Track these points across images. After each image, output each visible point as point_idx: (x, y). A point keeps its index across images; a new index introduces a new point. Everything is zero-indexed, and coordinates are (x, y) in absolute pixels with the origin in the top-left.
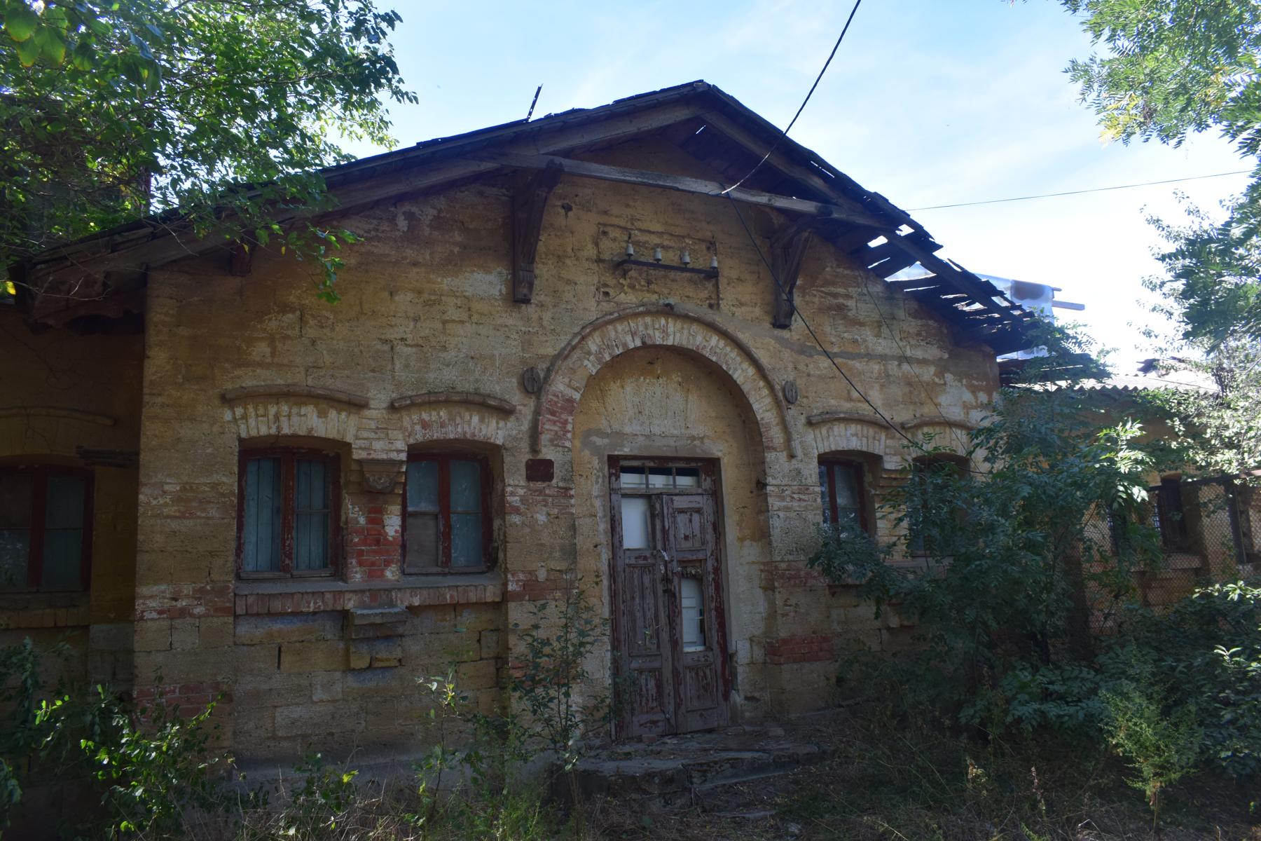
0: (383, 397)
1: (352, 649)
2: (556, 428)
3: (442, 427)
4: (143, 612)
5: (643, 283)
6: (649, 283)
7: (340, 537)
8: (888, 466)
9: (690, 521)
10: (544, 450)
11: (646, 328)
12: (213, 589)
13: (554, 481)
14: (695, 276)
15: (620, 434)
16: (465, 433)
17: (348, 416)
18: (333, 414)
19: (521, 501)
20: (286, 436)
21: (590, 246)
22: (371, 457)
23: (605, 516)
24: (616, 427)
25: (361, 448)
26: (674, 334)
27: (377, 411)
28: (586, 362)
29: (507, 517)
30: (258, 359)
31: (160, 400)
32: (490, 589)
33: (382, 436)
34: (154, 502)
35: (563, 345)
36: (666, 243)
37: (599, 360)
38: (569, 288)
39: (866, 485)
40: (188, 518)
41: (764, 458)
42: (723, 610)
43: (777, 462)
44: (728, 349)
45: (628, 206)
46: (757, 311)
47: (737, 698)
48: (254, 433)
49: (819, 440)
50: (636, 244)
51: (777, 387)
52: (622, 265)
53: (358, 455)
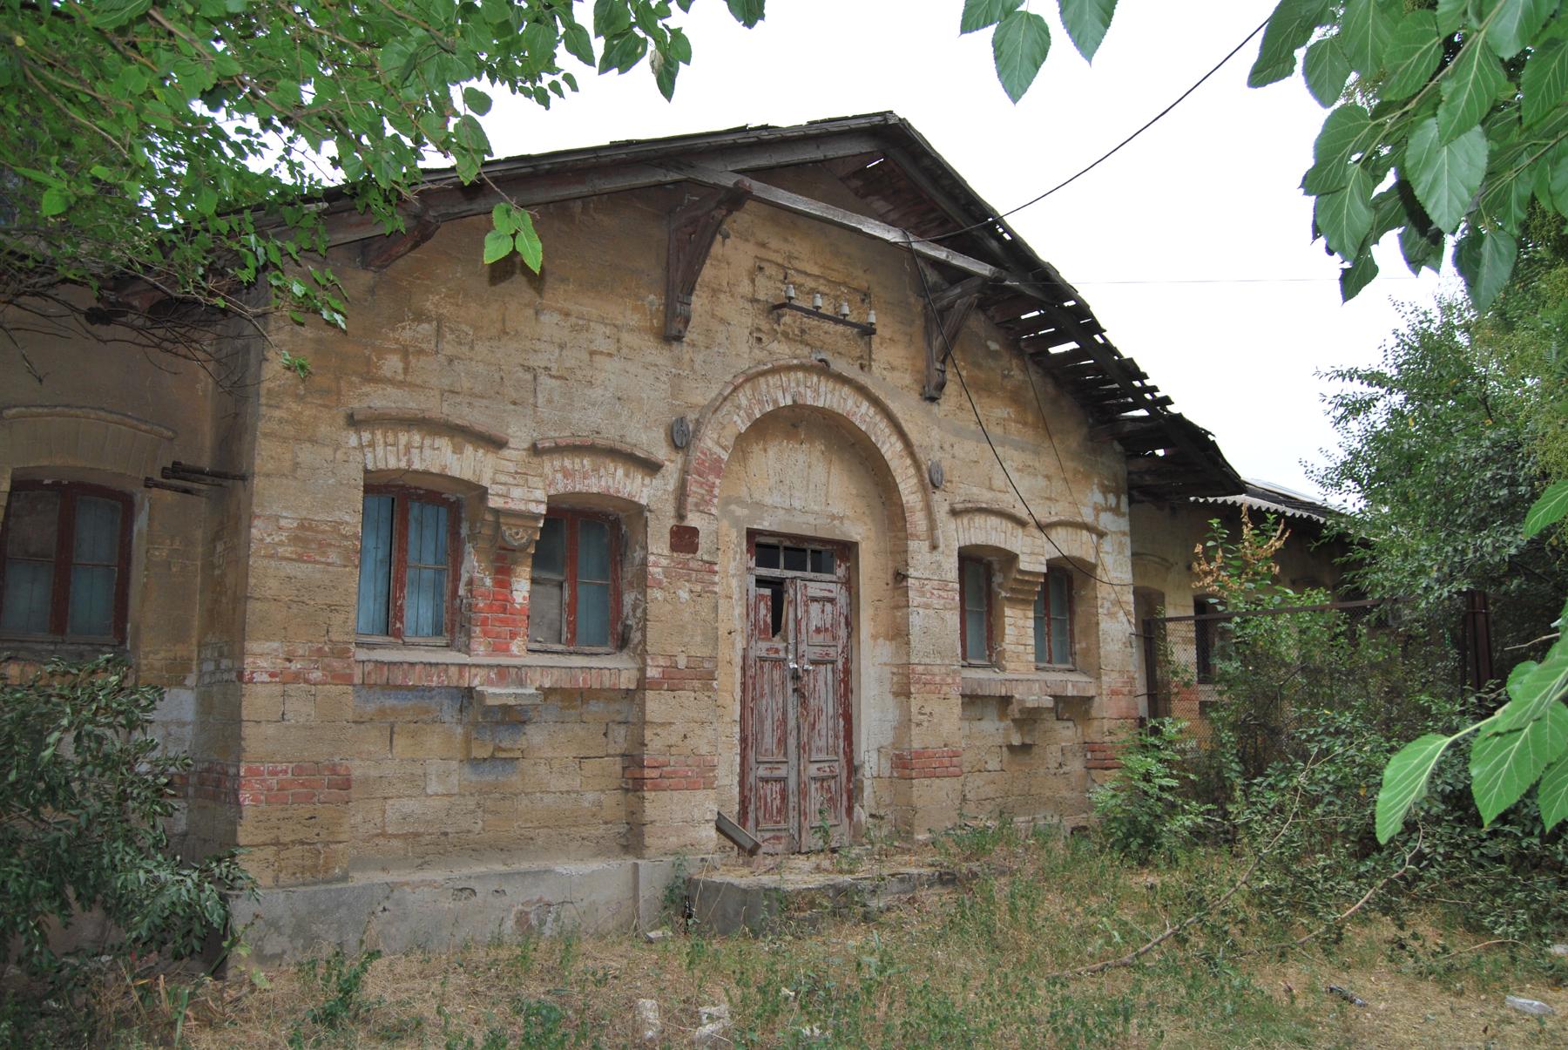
3: (585, 478)
4: (252, 673)
7: (458, 601)
8: (1023, 566)
9: (823, 611)
10: (690, 516)
11: (798, 385)
12: (332, 650)
14: (849, 331)
17: (485, 455)
18: (469, 449)
19: (664, 573)
20: (416, 472)
21: (746, 282)
22: (507, 506)
23: (740, 599)
24: (757, 496)
26: (825, 396)
27: (515, 453)
28: (736, 418)
29: (649, 591)
30: (389, 375)
31: (277, 413)
33: (522, 482)
34: (268, 540)
36: (822, 288)
38: (722, 328)
39: (995, 586)
40: (305, 562)
42: (851, 716)
43: (918, 548)
44: (878, 418)
45: (786, 240)
46: (907, 379)
47: (861, 814)
48: (382, 465)
49: (960, 530)
50: (798, 287)
53: (494, 502)
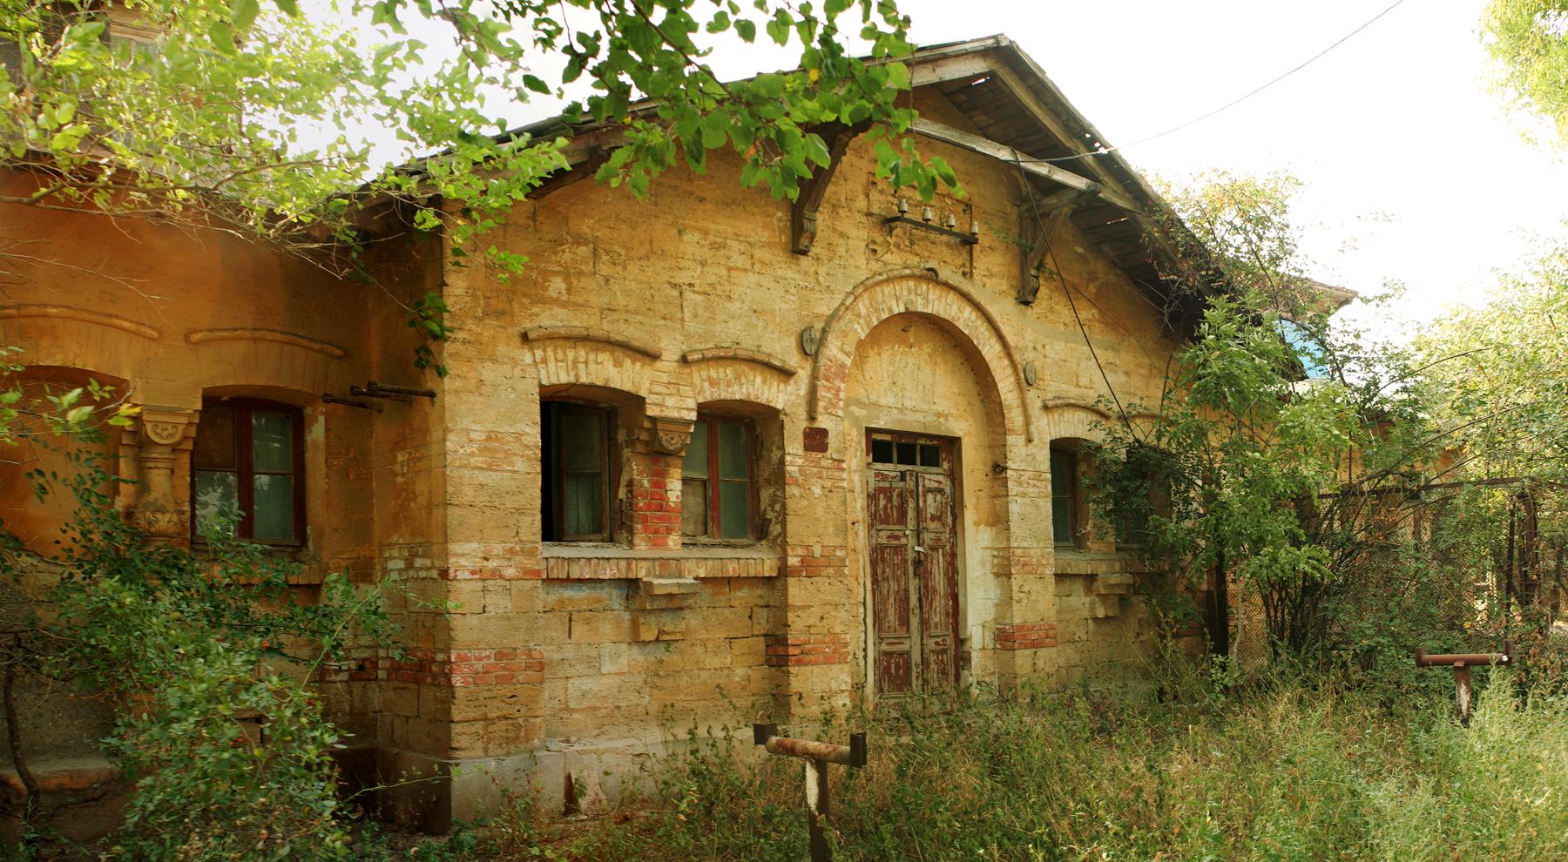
0: (674, 349)
1: (642, 620)
2: (829, 395)
5: (907, 243)
6: (912, 243)
10: (820, 418)
13: (829, 452)
14: (953, 240)
15: (876, 405)
16: (749, 394)
17: (642, 367)
18: (628, 363)
20: (583, 385)
21: (862, 197)
24: (873, 398)
25: (654, 404)
28: (856, 326)
30: (554, 295)
32: (768, 563)
34: (462, 451)
35: (836, 305)
37: (868, 323)
38: (841, 241)
41: (1005, 440)
43: (1015, 441)
46: (1005, 285)
48: (554, 381)
51: (1020, 369)
52: (888, 223)
53: (651, 411)
